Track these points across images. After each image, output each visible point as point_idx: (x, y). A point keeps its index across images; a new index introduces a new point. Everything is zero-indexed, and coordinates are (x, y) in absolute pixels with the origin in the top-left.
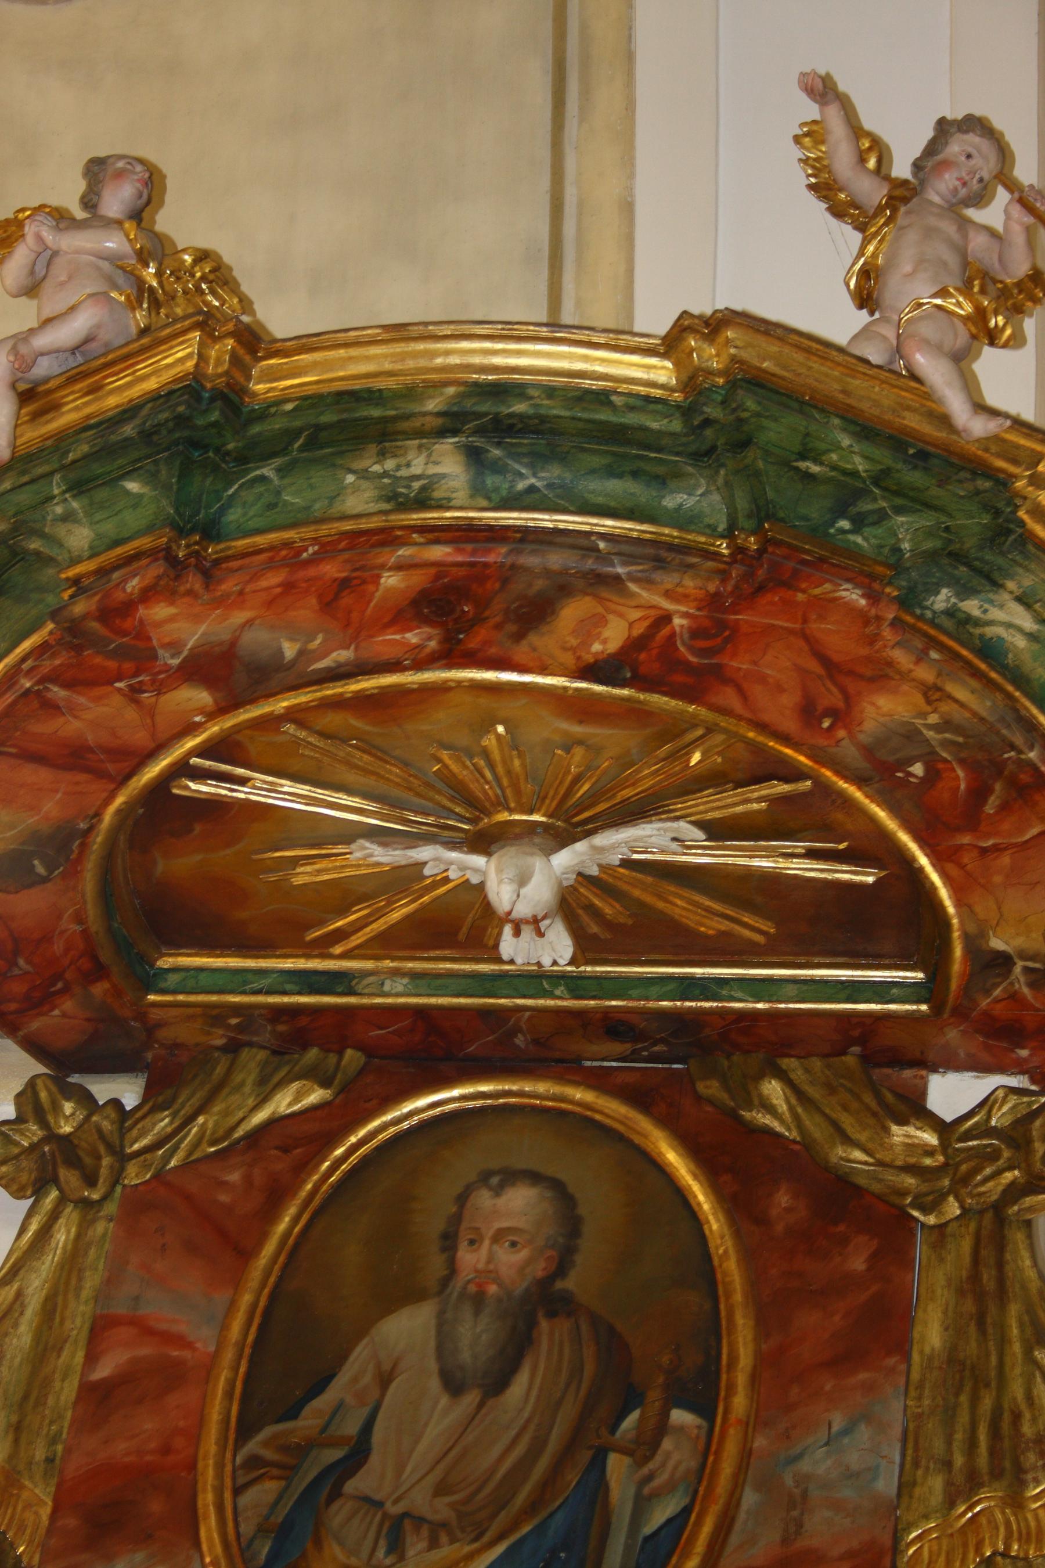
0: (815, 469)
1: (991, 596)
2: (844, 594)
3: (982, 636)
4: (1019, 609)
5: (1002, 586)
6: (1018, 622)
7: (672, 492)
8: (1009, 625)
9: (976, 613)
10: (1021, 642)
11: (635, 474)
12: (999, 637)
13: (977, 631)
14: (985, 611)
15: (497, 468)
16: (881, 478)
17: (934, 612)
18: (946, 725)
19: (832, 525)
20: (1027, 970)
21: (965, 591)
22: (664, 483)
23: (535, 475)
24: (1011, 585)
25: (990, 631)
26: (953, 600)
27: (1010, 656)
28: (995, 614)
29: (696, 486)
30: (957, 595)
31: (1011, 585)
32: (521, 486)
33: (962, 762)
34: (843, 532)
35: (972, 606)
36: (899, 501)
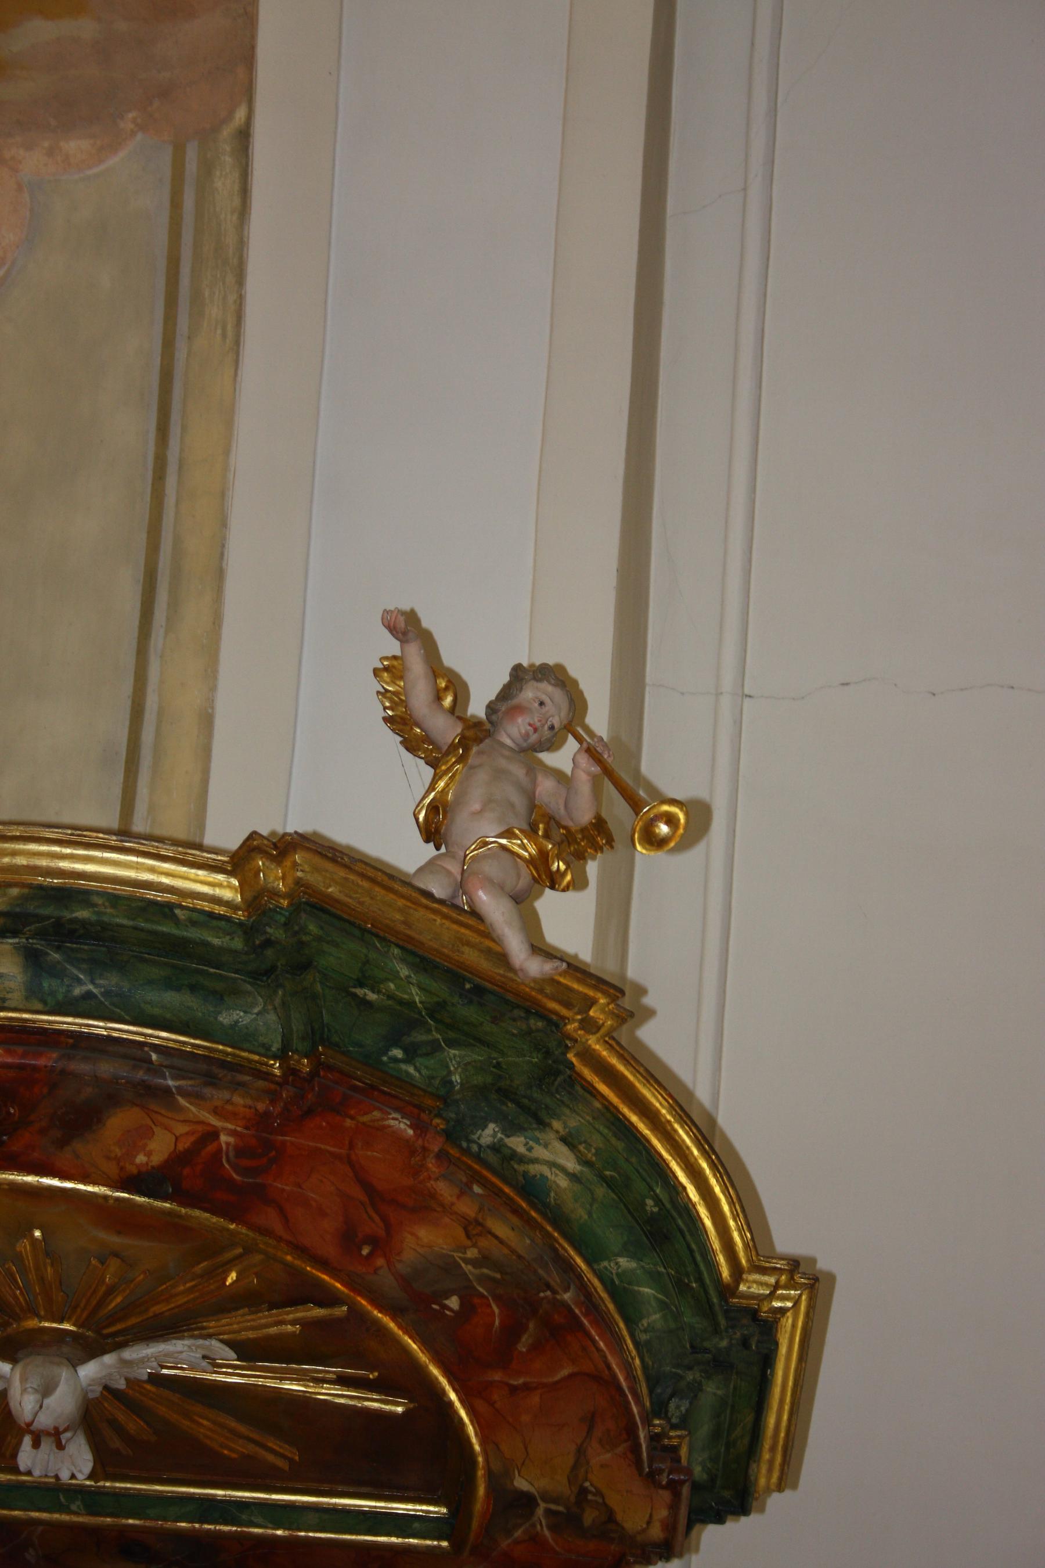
0: (372, 996)
1: (537, 1134)
2: (392, 1122)
3: (525, 1174)
4: (563, 1149)
5: (549, 1125)
6: (561, 1161)
7: (228, 1009)
8: (552, 1165)
9: (521, 1150)
10: (563, 1182)
11: (193, 988)
12: (542, 1175)
13: (521, 1168)
14: (530, 1149)
15: (56, 972)
16: (436, 1010)
17: (480, 1146)
18: (485, 1260)
19: (385, 1053)
20: (548, 1512)
21: (512, 1128)
22: (222, 998)
23: (92, 982)
24: (556, 1125)
25: (533, 1169)
26: (499, 1135)
27: (552, 1194)
28: (540, 1152)
29: (254, 1005)
30: (503, 1131)
31: (556, 1125)
32: (77, 991)
33: (498, 1298)
34: (395, 1060)
35: (517, 1143)
36: (452, 1035)
